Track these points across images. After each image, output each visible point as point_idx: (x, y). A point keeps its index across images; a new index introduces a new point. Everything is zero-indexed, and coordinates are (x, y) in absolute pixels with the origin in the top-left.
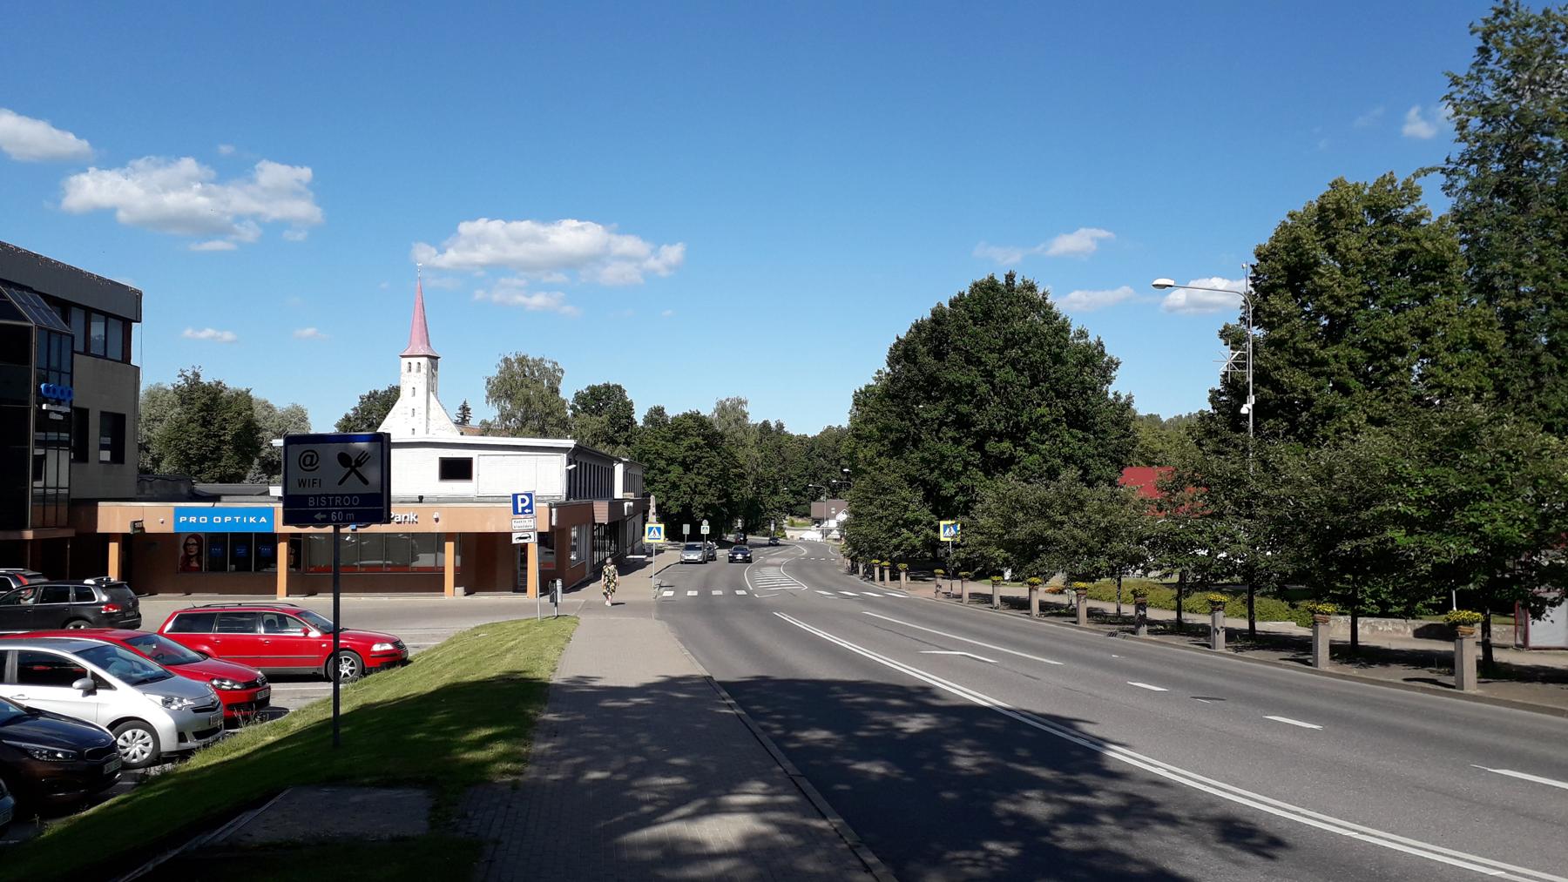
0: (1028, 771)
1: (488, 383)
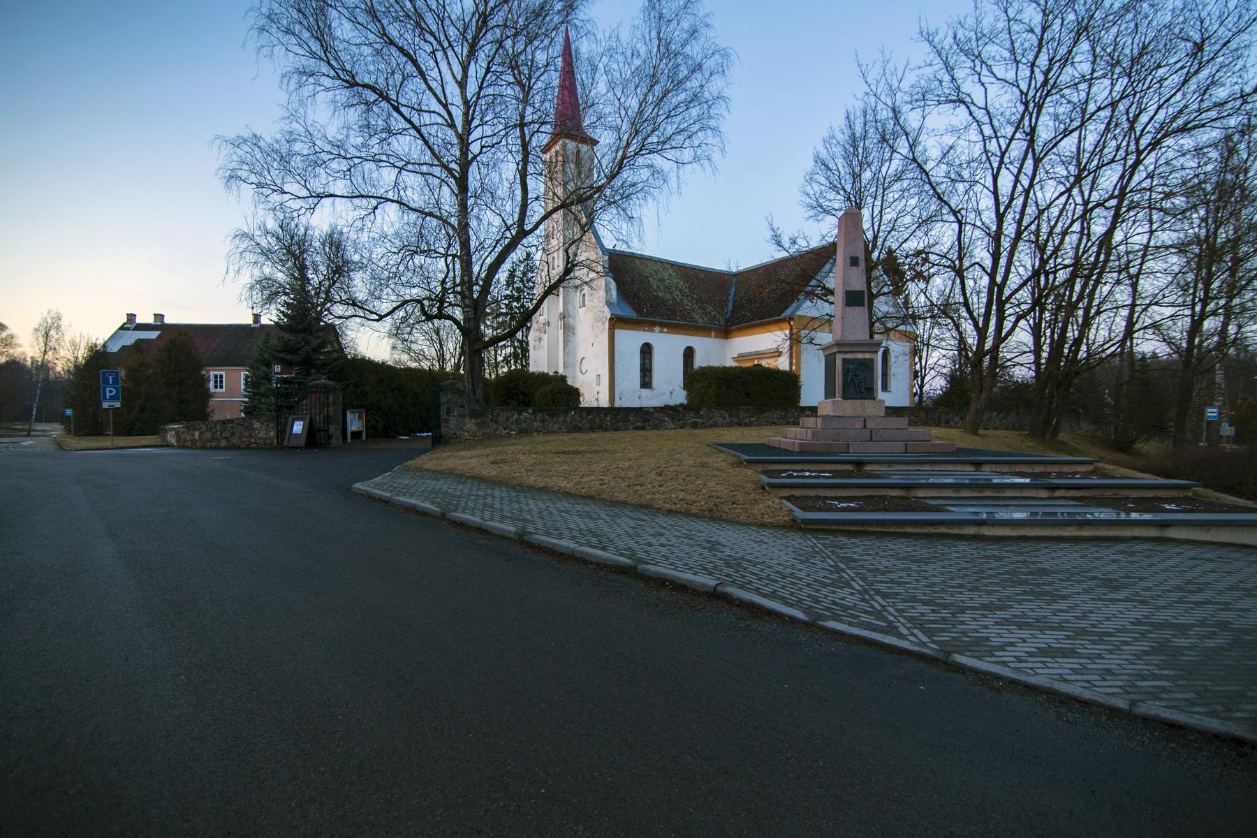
0: (401, 501)
1: (574, 333)
